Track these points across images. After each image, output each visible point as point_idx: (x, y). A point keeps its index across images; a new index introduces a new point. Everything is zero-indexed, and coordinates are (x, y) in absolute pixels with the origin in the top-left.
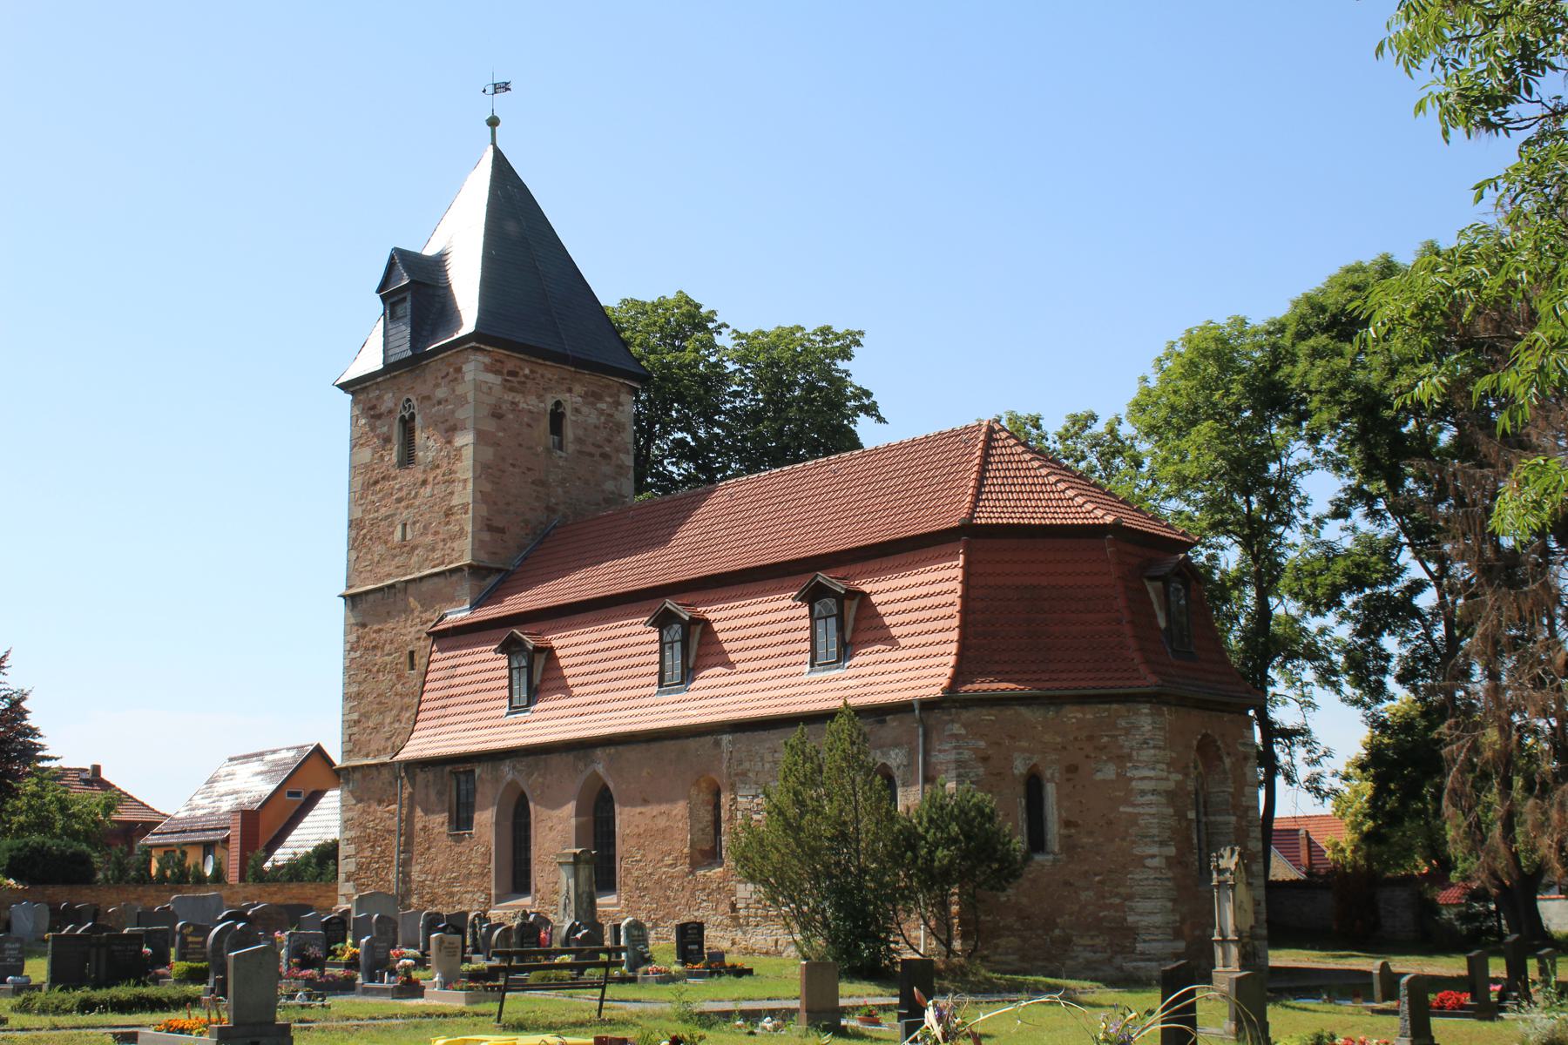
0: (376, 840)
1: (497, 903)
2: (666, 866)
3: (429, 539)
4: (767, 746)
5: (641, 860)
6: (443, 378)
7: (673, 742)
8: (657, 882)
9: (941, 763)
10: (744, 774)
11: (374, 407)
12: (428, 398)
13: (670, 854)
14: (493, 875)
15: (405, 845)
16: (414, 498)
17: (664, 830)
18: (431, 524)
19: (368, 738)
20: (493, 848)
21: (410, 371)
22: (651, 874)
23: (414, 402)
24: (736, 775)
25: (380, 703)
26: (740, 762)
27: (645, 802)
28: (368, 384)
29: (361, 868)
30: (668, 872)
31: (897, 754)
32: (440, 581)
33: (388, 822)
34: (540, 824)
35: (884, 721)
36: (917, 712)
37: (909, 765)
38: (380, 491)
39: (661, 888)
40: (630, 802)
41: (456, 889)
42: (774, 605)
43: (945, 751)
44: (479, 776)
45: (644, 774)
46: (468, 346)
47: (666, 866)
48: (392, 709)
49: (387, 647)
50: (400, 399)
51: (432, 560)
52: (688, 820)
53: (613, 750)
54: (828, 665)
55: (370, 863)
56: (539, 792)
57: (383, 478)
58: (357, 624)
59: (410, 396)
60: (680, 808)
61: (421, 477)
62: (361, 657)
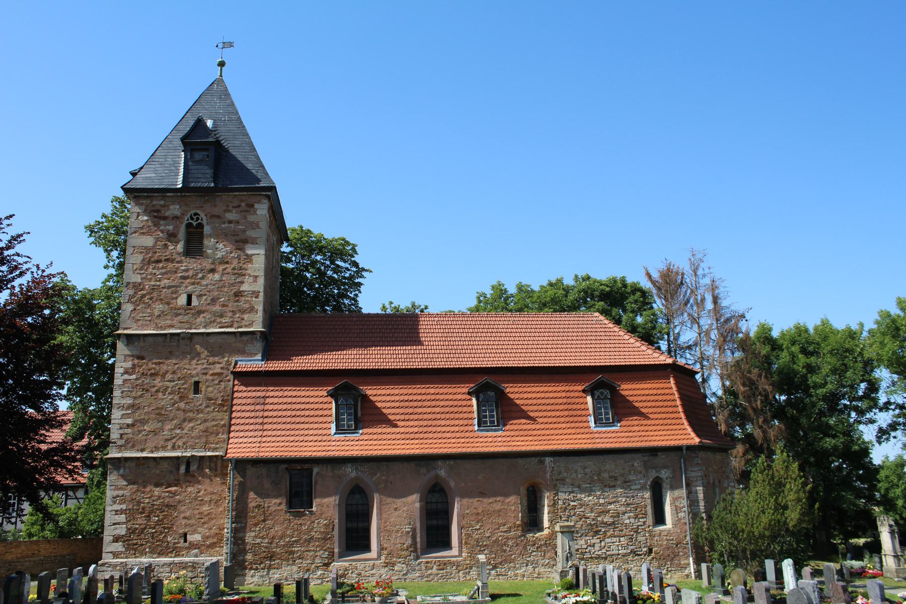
0: (151, 512)
1: (340, 557)
2: (502, 532)
3: (217, 308)
4: (580, 464)
5: (479, 529)
6: (233, 207)
7: (505, 460)
8: (495, 542)
9: (693, 477)
10: (563, 480)
11: (158, 211)
12: (219, 217)
13: (505, 525)
14: (336, 539)
15: (235, 518)
16: (200, 279)
17: (499, 511)
18: (219, 298)
19: (144, 438)
20: (336, 521)
21: (201, 196)
22: (489, 537)
23: (202, 215)
24: (556, 480)
25: (159, 414)
26: (560, 473)
27: (482, 494)
28: (156, 194)
29: (133, 532)
30: (504, 536)
31: (666, 472)
32: (232, 339)
33: (168, 500)
34: (384, 507)
35: (657, 455)
36: (684, 451)
37: (673, 477)
38: (163, 268)
39: (499, 545)
40: (466, 494)
41: (296, 549)
42: (546, 389)
43: (694, 471)
44: (317, 473)
45: (480, 477)
46: (263, 193)
47: (502, 532)
48: (173, 420)
49: (169, 376)
50: (187, 211)
51: (219, 323)
52: (519, 506)
53: (452, 462)
54: (608, 424)
55: (145, 528)
56: (383, 486)
57: (167, 260)
58: (132, 356)
59: (198, 212)
60: (512, 499)
61: (209, 267)
62: (137, 379)
